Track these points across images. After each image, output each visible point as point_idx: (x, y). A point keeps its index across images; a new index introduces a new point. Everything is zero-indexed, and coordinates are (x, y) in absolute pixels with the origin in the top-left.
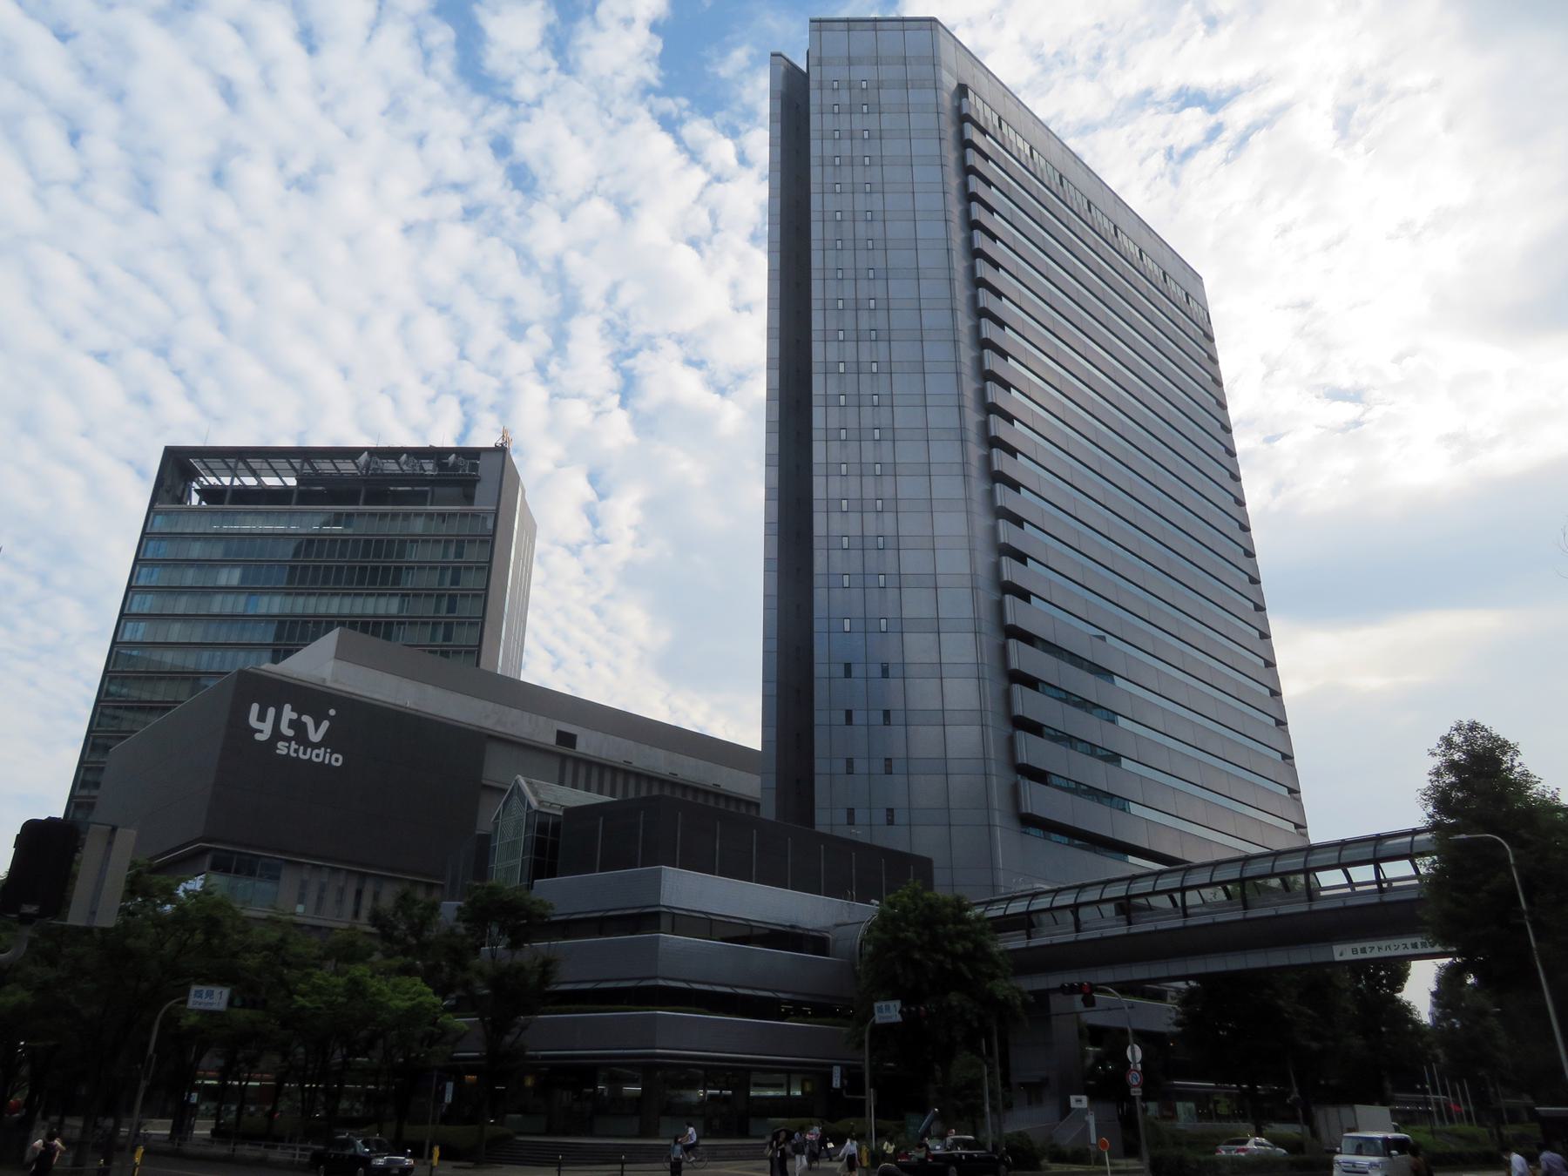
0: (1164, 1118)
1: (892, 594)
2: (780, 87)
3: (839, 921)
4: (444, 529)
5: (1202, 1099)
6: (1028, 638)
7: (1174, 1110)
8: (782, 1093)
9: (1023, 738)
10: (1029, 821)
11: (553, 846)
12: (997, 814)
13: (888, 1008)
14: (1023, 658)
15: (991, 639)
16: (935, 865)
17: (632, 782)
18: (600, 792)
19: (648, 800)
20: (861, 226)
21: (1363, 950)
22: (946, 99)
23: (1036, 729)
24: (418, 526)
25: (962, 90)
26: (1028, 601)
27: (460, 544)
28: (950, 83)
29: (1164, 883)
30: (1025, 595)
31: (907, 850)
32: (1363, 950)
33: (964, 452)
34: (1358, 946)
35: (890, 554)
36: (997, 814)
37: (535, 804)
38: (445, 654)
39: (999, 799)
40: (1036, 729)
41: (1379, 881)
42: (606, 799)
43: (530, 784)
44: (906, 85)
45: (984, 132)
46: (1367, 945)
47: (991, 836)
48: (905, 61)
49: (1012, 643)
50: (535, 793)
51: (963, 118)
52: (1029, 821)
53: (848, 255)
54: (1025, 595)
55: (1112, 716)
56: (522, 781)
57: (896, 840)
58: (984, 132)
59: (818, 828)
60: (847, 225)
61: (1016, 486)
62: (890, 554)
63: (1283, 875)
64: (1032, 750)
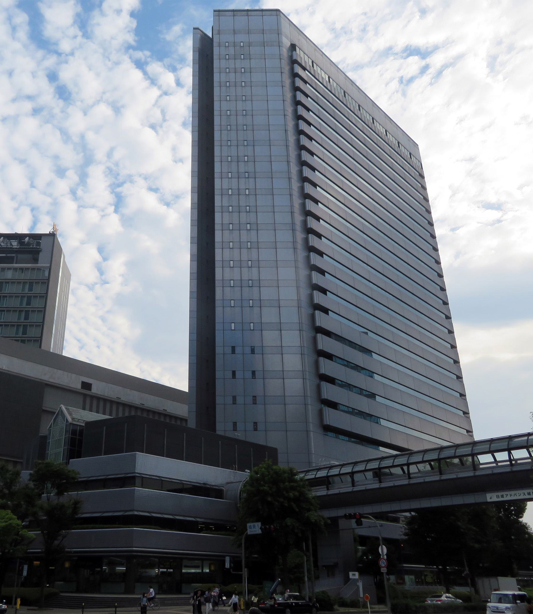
0: (398, 584)
1: (256, 310)
2: (198, 45)
3: (229, 481)
4: (23, 276)
5: (418, 574)
6: (328, 333)
7: (403, 580)
8: (199, 571)
9: (325, 386)
10: (327, 429)
11: (80, 441)
12: (311, 425)
13: (254, 527)
14: (325, 343)
15: (308, 334)
16: (279, 451)
17: (121, 409)
18: (104, 414)
19: (129, 418)
20: (240, 118)
21: (502, 496)
22: (285, 52)
23: (331, 380)
24: (9, 275)
25: (293, 47)
26: (328, 314)
27: (31, 284)
28: (287, 43)
29: (398, 461)
30: (326, 311)
31: (264, 444)
32: (502, 496)
33: (294, 236)
34: (500, 494)
35: (256, 290)
36: (311, 425)
37: (70, 420)
38: (23, 341)
39: (312, 417)
40: (331, 380)
41: (510, 460)
42: (107, 417)
43: (67, 409)
44: (264, 44)
45: (304, 69)
46: (504, 493)
47: (308, 436)
48: (263, 32)
49: (321, 359)
50: (70, 414)
51: (293, 62)
52: (327, 429)
53: (233, 133)
54: (326, 311)
55: (371, 374)
56: (63, 408)
57: (258, 439)
58: (304, 69)
59: (218, 433)
60: (233, 118)
61: (321, 254)
62: (256, 290)
63: (460, 457)
64: (330, 392)
